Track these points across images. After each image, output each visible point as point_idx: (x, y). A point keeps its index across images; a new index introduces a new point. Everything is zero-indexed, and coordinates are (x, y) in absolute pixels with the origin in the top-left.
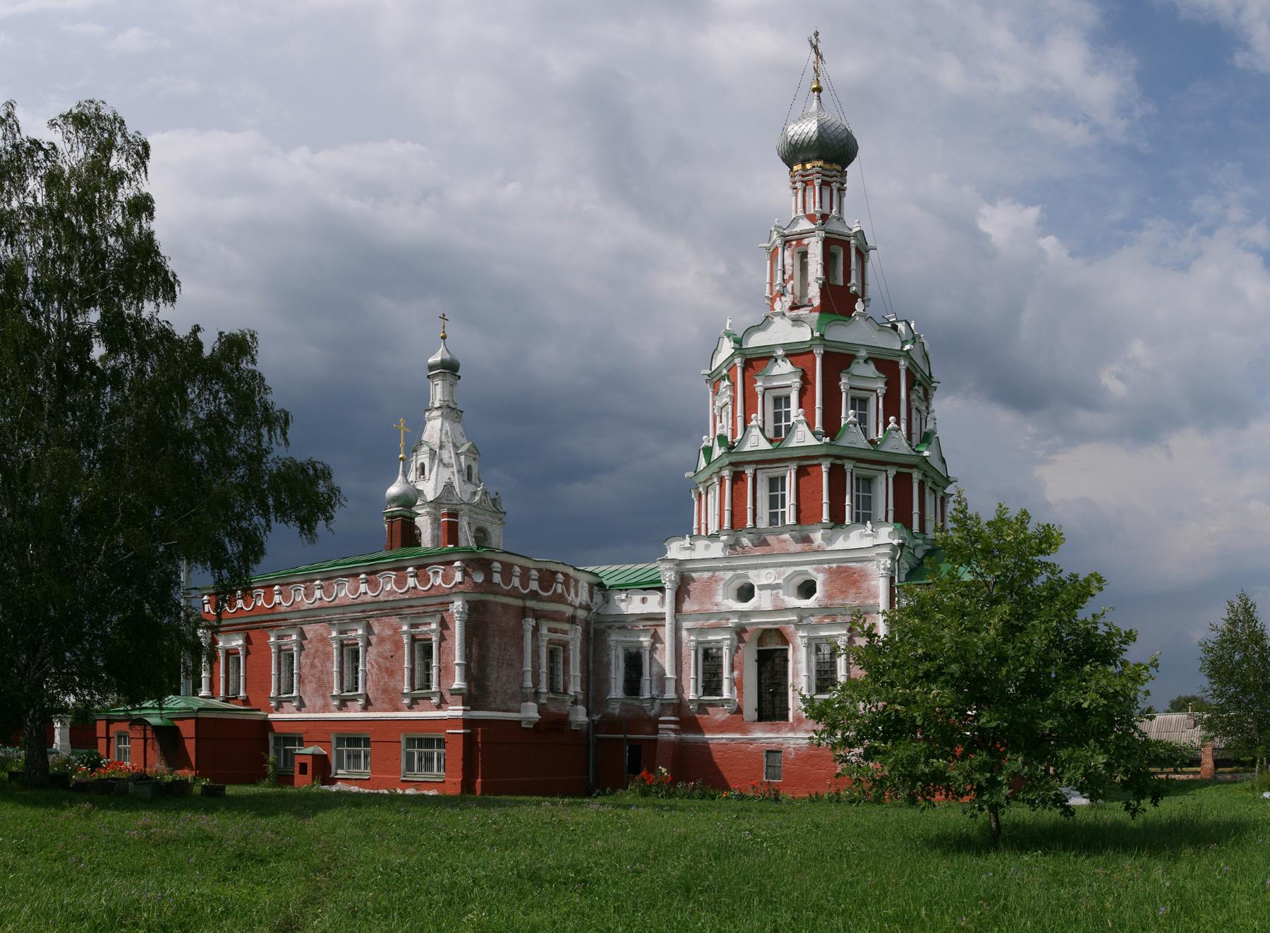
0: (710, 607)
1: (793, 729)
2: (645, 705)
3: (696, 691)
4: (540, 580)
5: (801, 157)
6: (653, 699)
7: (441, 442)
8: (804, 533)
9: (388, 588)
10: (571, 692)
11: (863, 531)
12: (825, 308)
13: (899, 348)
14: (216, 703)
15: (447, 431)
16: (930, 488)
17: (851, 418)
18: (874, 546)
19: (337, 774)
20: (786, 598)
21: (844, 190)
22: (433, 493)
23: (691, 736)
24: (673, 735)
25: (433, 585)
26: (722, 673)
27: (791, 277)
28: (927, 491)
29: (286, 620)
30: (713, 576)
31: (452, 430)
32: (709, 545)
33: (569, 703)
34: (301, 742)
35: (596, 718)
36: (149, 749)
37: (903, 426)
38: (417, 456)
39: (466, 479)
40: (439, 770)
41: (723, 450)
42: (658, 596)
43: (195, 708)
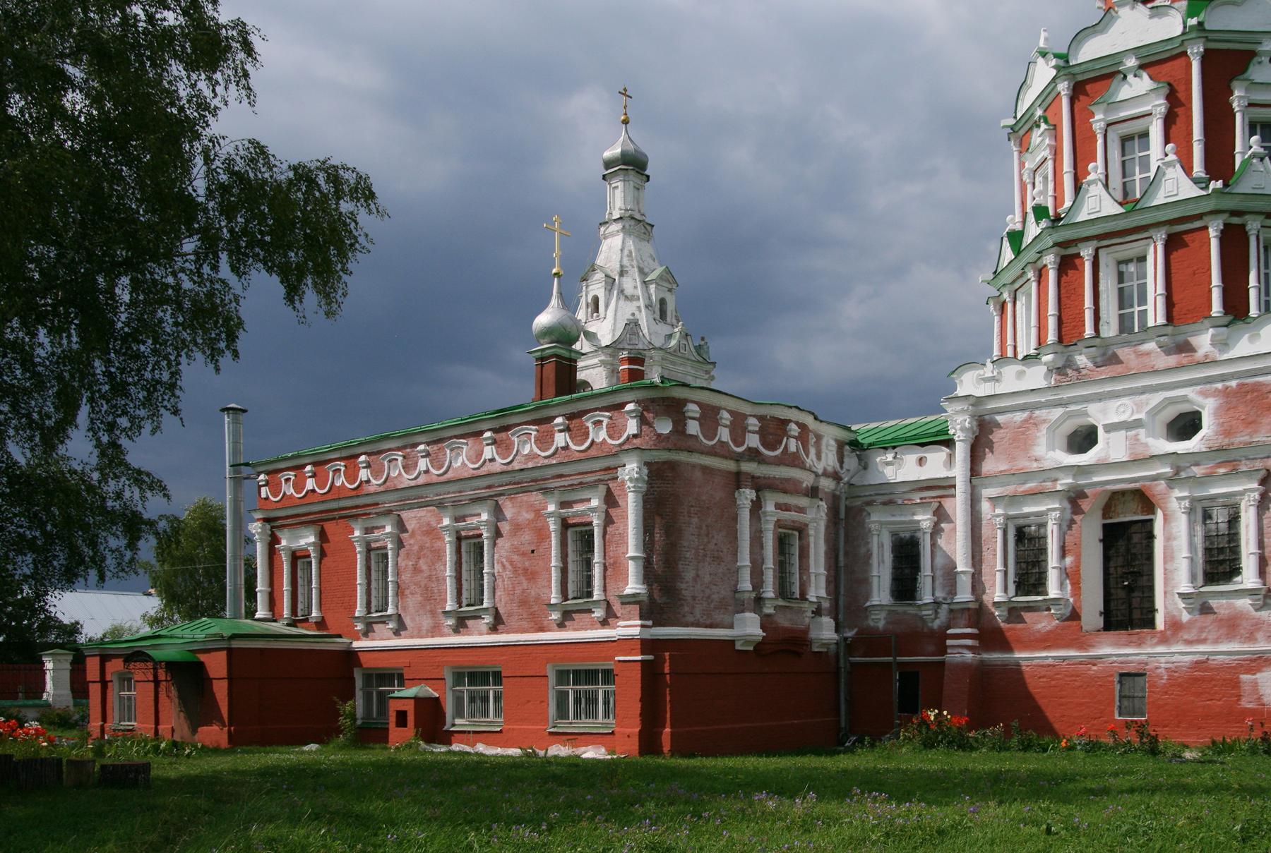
0: (1027, 464)
1: (1164, 639)
2: (924, 613)
3: (1006, 589)
4: (762, 433)
6: (937, 603)
7: (622, 266)
8: (1180, 339)
9: (526, 451)
14: (279, 627)
15: (631, 252)
19: (454, 725)
20: (1151, 441)
22: (610, 337)
23: (996, 656)
24: (969, 656)
25: (593, 442)
26: (1046, 561)
29: (378, 504)
30: (1030, 418)
31: (638, 250)
33: (809, 614)
34: (402, 682)
35: (850, 634)
36: (162, 696)
38: (587, 287)
39: (658, 317)
40: (606, 715)
41: (1044, 224)
42: (943, 452)
43: (227, 634)
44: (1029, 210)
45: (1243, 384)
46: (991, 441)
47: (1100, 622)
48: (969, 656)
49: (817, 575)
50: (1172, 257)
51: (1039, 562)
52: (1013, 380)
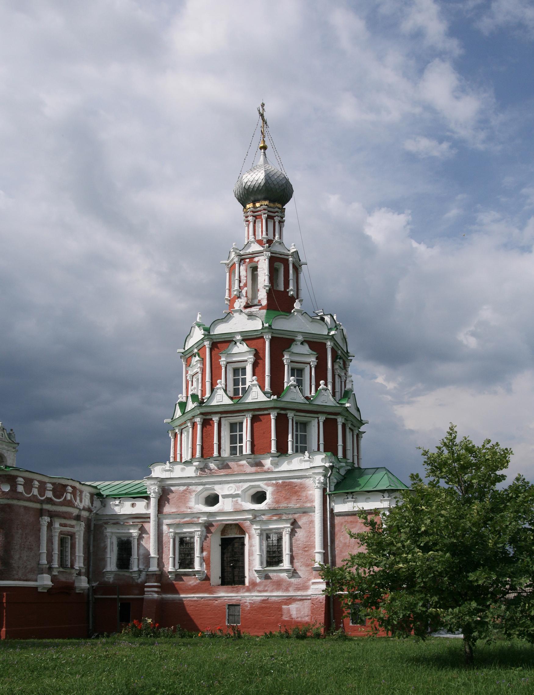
0: (185, 510)
1: (248, 590)
2: (133, 575)
3: (174, 566)
4: (54, 491)
5: (252, 198)
6: (140, 571)
8: (257, 460)
10: (77, 566)
11: (302, 458)
12: (270, 306)
13: (326, 334)
16: (350, 428)
17: (292, 382)
18: (311, 468)
20: (243, 503)
21: (283, 222)
24: (156, 596)
26: (194, 553)
27: (245, 285)
28: (348, 430)
30: (187, 489)
32: (185, 468)
33: (75, 575)
35: (95, 584)
37: (330, 387)
41: (196, 404)
42: (145, 502)
44: (189, 395)
45: (284, 482)
46: (168, 498)
47: (220, 582)
48: (156, 596)
49: (79, 556)
50: (254, 425)
51: (190, 554)
52: (178, 472)
